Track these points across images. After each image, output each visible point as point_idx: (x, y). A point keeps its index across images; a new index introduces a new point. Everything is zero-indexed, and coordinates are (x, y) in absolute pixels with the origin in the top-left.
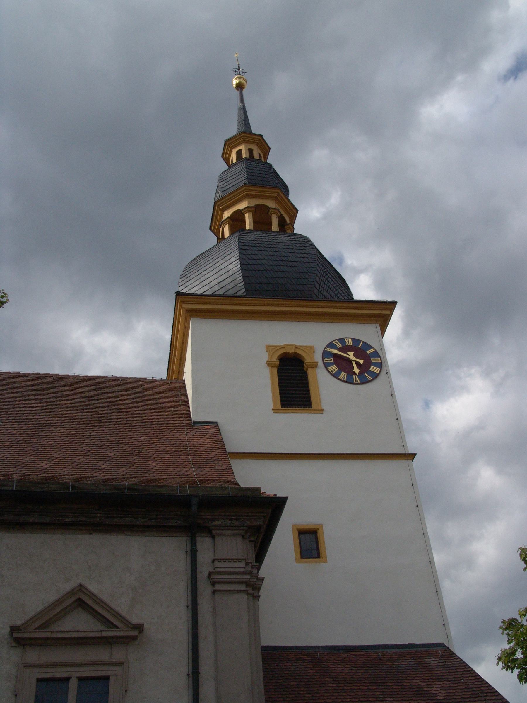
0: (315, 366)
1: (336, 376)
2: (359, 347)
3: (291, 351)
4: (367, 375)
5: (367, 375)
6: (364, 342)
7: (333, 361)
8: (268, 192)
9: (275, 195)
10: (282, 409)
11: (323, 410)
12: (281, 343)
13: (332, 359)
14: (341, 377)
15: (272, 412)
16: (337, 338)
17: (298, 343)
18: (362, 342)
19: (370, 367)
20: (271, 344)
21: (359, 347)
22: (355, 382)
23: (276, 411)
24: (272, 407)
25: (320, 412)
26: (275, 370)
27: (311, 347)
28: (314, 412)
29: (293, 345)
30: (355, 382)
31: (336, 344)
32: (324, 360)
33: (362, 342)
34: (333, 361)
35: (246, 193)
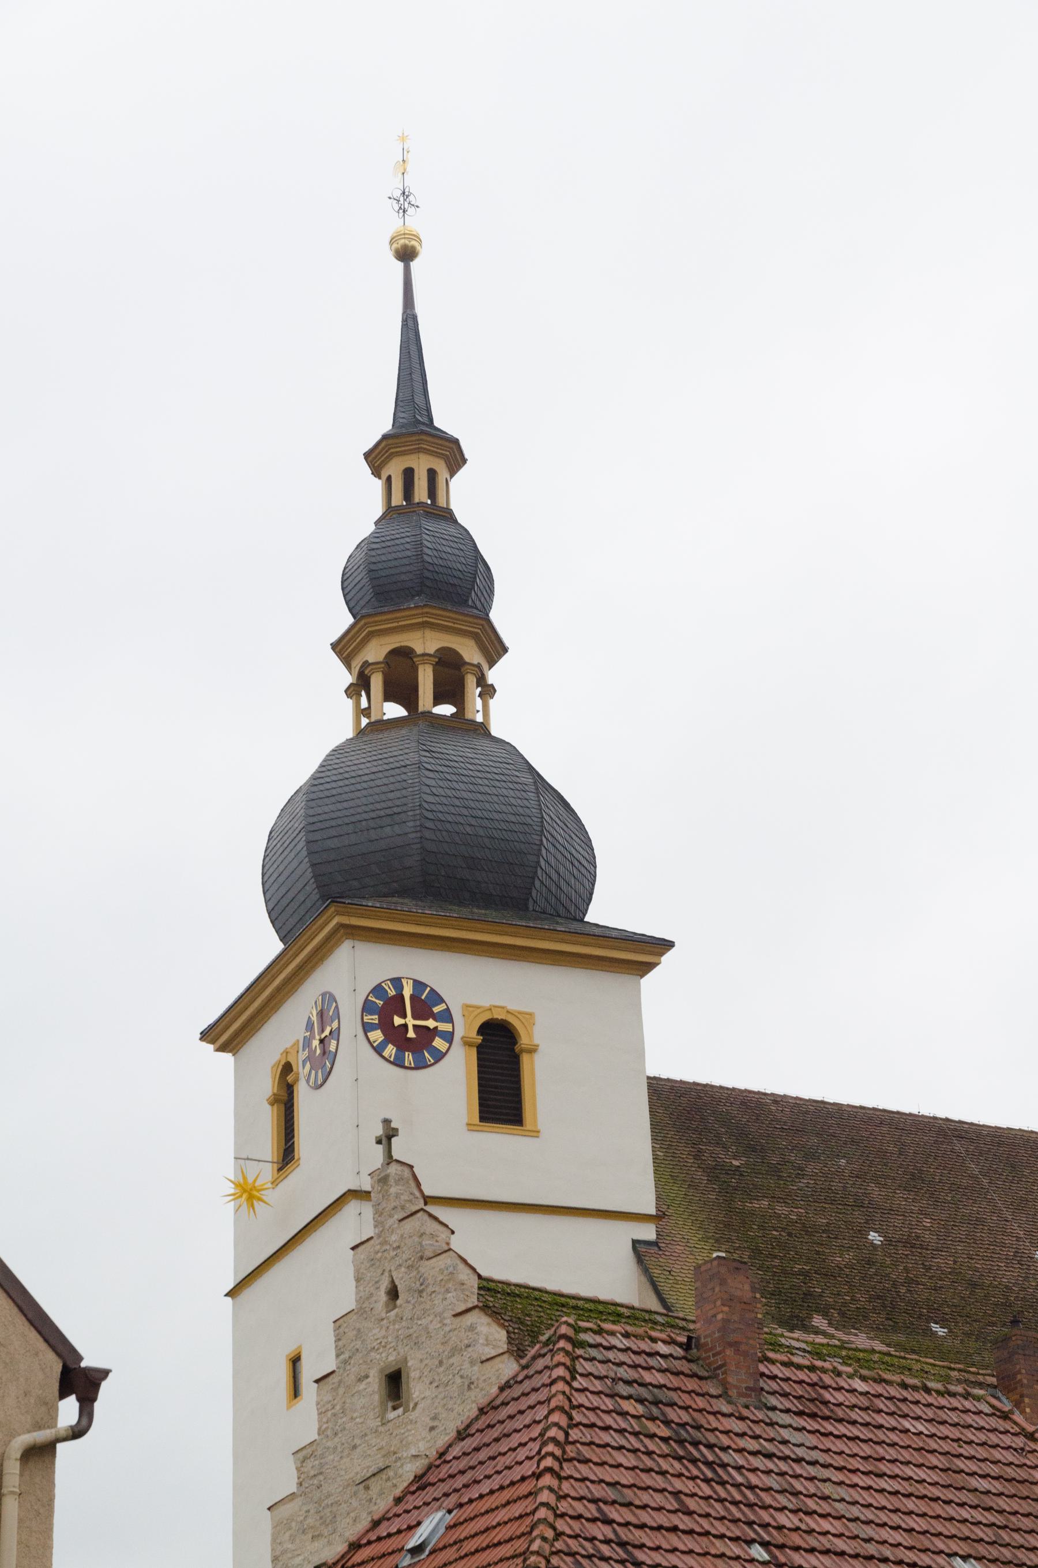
0: (467, 1043)
1: (379, 1050)
2: (423, 997)
3: (499, 1015)
4: (426, 1054)
5: (426, 1054)
6: (432, 990)
7: (377, 1022)
8: (442, 616)
9: (476, 630)
10: (482, 1124)
11: (538, 1132)
12: (486, 1003)
13: (377, 1017)
14: (386, 1054)
15: (465, 1128)
16: (390, 977)
17: (512, 1007)
18: (429, 989)
19: (433, 1041)
20: (469, 1002)
21: (423, 997)
22: (406, 1064)
23: (472, 1128)
24: (466, 1121)
25: (535, 1134)
26: (474, 1051)
27: (531, 1014)
28: (527, 1133)
29: (503, 1008)
30: (406, 1064)
31: (387, 988)
32: (365, 1018)
33: (429, 989)
34: (377, 1022)
35: (479, 631)
